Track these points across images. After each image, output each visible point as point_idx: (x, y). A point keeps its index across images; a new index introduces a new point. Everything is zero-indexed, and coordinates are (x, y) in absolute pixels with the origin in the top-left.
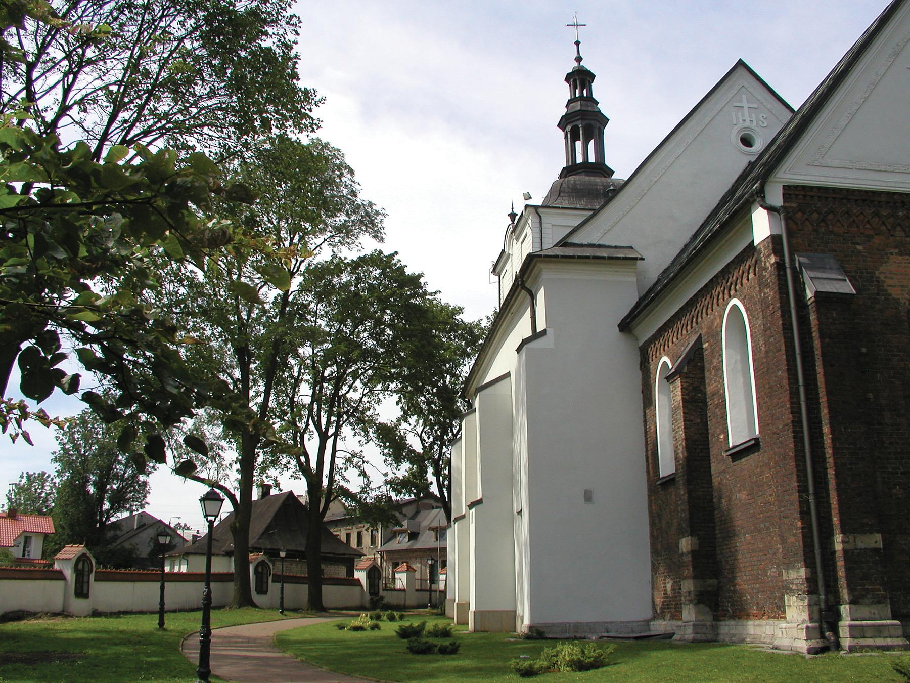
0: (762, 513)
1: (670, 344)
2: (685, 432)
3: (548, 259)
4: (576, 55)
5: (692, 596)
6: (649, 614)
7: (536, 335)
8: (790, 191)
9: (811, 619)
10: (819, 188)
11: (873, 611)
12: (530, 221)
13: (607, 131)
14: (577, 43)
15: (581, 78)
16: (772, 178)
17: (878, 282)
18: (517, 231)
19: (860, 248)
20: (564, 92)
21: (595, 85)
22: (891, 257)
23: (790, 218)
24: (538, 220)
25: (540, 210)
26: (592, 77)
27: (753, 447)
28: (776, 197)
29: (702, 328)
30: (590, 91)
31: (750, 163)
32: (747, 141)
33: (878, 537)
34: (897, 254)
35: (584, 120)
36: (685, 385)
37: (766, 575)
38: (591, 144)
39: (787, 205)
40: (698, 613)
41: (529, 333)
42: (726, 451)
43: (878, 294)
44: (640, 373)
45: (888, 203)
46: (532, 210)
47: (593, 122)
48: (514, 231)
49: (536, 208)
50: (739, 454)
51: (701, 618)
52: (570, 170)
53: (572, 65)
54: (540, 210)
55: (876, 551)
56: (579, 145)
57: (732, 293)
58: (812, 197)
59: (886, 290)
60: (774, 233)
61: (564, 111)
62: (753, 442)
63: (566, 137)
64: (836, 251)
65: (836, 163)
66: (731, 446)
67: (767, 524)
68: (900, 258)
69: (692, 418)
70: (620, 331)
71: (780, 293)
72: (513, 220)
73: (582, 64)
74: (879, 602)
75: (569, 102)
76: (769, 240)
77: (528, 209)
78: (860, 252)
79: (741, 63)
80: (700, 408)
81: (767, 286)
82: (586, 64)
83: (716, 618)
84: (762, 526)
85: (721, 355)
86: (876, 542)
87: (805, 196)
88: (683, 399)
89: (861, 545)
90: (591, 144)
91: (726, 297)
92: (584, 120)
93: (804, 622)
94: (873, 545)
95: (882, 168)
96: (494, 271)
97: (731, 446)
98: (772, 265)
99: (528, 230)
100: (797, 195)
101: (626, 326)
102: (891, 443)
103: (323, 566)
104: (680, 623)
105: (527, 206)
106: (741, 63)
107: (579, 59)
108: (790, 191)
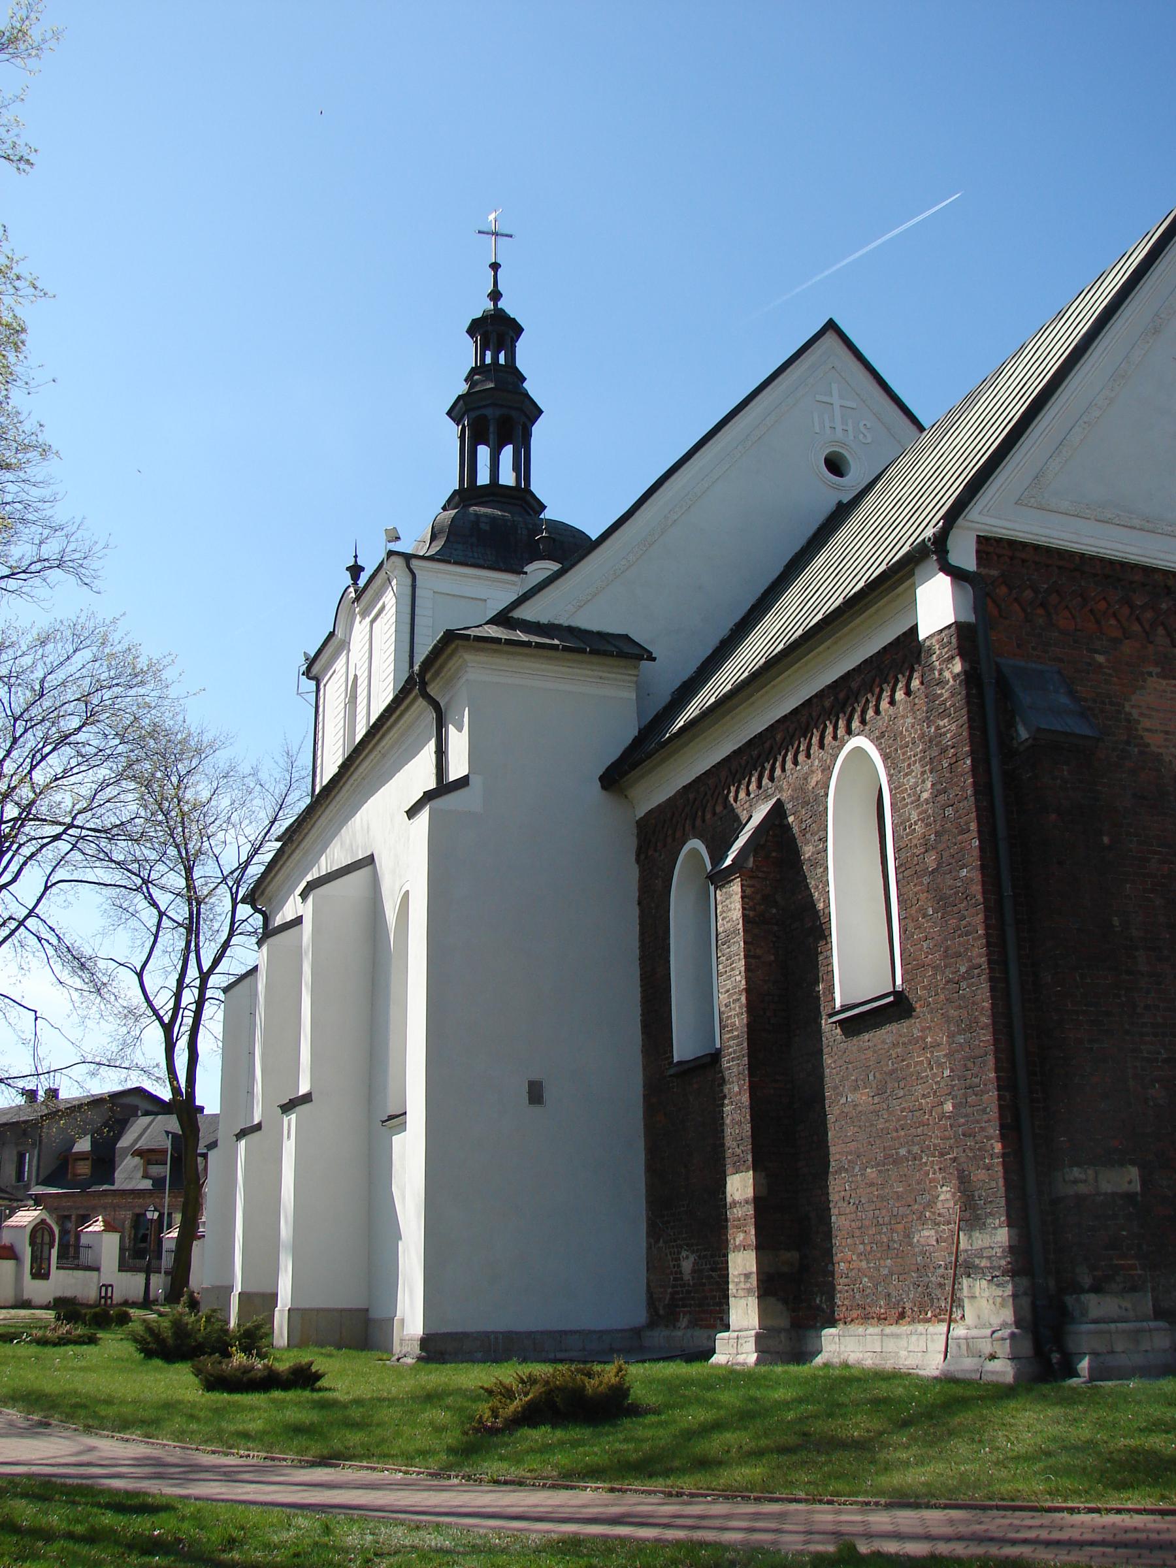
0: (912, 1126)
1: (708, 816)
2: (747, 979)
3: (482, 645)
6: (640, 1317)
7: (444, 788)
8: (987, 546)
9: (1018, 1323)
10: (1037, 548)
11: (1124, 1304)
12: (394, 582)
13: (539, 430)
14: (495, 266)
15: (496, 330)
16: (960, 521)
17: (1128, 721)
19: (1100, 659)
20: (465, 354)
22: (1149, 679)
23: (988, 595)
24: (409, 581)
25: (415, 563)
26: (518, 330)
27: (896, 1008)
28: (964, 555)
29: (781, 790)
30: (511, 356)
31: (840, 504)
33: (1134, 1172)
34: (1158, 676)
35: (496, 408)
36: (748, 891)
37: (911, 1244)
38: (507, 453)
39: (984, 571)
41: (432, 784)
42: (830, 1016)
43: (1128, 743)
44: (633, 873)
45: (1144, 585)
46: (399, 562)
47: (514, 414)
48: (358, 599)
49: (408, 557)
50: (859, 1023)
52: (466, 495)
54: (415, 563)
55: (1130, 1197)
56: (483, 452)
57: (855, 724)
58: (1023, 561)
59: (1142, 738)
60: (962, 620)
61: (463, 388)
62: (891, 999)
63: (462, 438)
64: (1061, 660)
66: (838, 1005)
67: (916, 1149)
68: (1164, 682)
69: (759, 952)
70: (604, 787)
71: (970, 727)
73: (500, 305)
74: (1134, 1289)
75: (474, 371)
76: (953, 629)
77: (393, 558)
78: (1100, 666)
79: (831, 326)
80: (789, 929)
81: (943, 714)
84: (903, 1152)
85: (824, 840)
86: (1130, 1182)
87: (1012, 558)
88: (744, 916)
89: (1106, 1187)
90: (507, 453)
91: (841, 732)
92: (496, 408)
93: (1004, 1325)
94: (1125, 1188)
95: (1136, 522)
96: (307, 673)
97: (838, 1005)
98: (955, 677)
99: (389, 599)
100: (999, 556)
101: (614, 778)
102: (1147, 1007)
105: (391, 553)
106: (831, 326)
107: (495, 295)
108: (987, 546)
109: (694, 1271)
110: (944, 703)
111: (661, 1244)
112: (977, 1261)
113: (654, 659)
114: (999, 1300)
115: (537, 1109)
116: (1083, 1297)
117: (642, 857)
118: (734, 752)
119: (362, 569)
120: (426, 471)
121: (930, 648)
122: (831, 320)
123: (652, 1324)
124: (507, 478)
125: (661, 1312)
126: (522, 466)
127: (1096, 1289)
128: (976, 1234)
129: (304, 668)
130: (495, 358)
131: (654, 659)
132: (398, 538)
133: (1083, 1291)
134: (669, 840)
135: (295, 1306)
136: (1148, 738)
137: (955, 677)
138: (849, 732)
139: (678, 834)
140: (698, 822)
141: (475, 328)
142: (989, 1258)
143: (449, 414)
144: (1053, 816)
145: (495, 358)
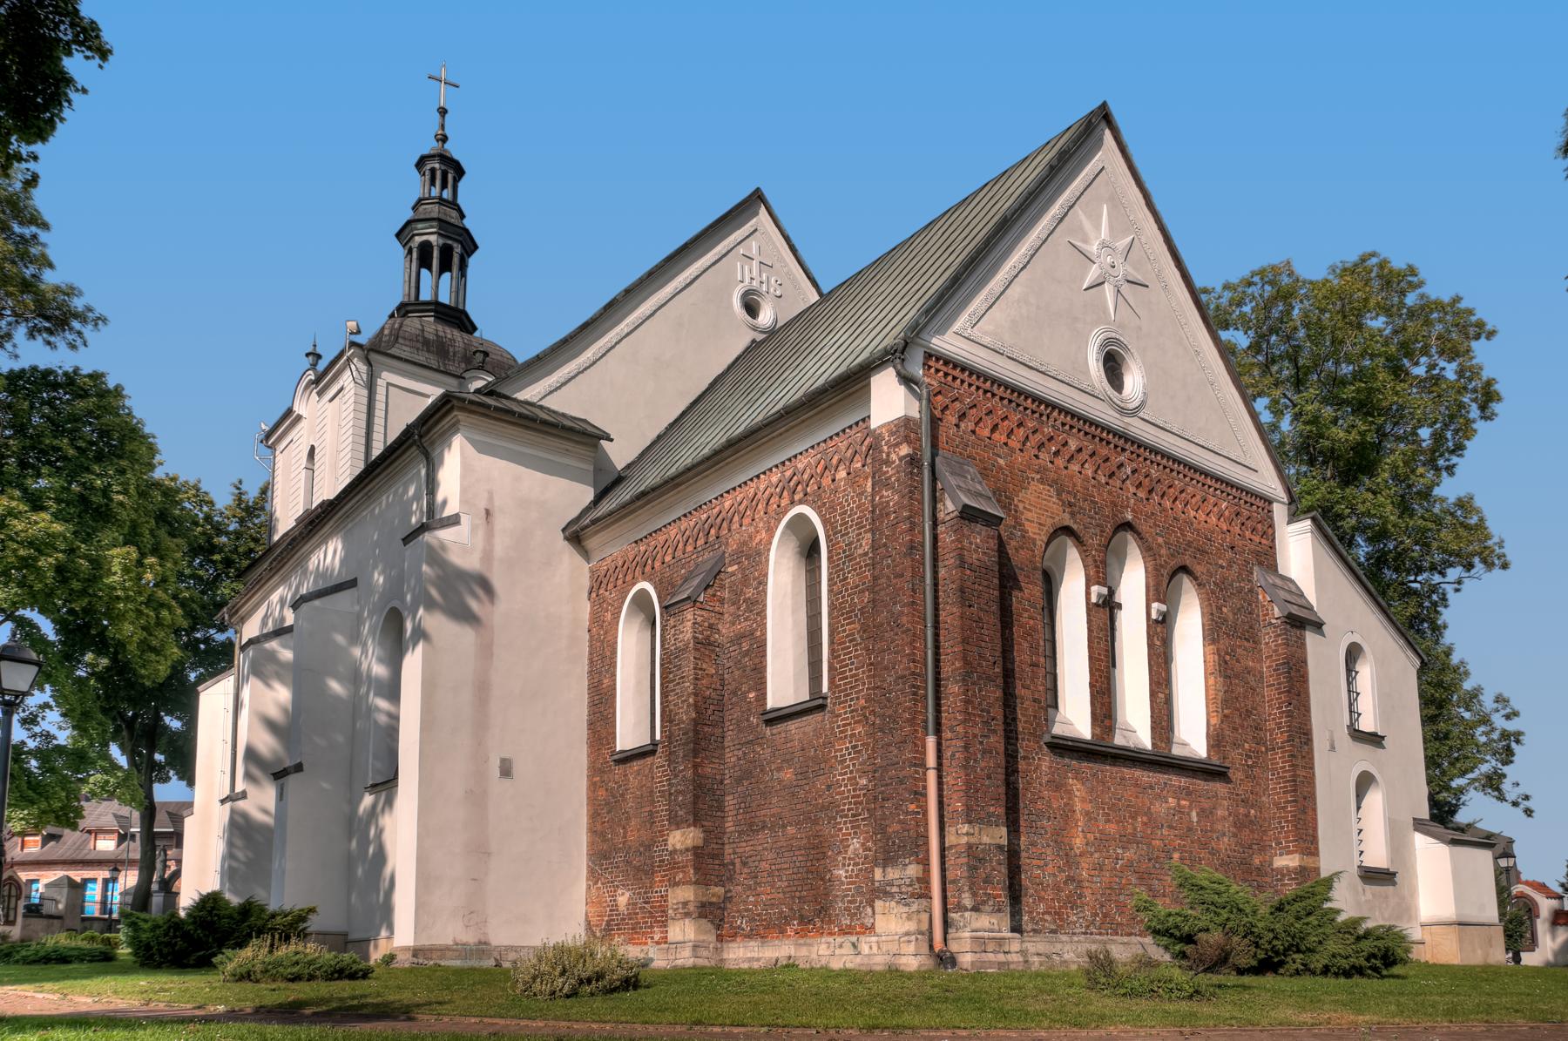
4: (436, 129)
5: (691, 908)
14: (443, 112)
15: (444, 168)
19: (1001, 462)
27: (815, 706)
32: (751, 309)
40: (698, 931)
51: (702, 938)
53: (429, 146)
55: (1000, 847)
65: (986, 340)
74: (999, 910)
81: (888, 486)
82: (454, 149)
83: (720, 938)
87: (946, 374)
97: (769, 706)
103: (1448, 490)
105: (353, 344)
115: (507, 782)
120: (380, 282)
122: (758, 190)
124: (445, 298)
126: (460, 288)
128: (889, 869)
134: (620, 582)
135: (425, 942)
136: (1028, 526)
138: (793, 503)
139: (629, 578)
140: (648, 568)
143: (398, 235)
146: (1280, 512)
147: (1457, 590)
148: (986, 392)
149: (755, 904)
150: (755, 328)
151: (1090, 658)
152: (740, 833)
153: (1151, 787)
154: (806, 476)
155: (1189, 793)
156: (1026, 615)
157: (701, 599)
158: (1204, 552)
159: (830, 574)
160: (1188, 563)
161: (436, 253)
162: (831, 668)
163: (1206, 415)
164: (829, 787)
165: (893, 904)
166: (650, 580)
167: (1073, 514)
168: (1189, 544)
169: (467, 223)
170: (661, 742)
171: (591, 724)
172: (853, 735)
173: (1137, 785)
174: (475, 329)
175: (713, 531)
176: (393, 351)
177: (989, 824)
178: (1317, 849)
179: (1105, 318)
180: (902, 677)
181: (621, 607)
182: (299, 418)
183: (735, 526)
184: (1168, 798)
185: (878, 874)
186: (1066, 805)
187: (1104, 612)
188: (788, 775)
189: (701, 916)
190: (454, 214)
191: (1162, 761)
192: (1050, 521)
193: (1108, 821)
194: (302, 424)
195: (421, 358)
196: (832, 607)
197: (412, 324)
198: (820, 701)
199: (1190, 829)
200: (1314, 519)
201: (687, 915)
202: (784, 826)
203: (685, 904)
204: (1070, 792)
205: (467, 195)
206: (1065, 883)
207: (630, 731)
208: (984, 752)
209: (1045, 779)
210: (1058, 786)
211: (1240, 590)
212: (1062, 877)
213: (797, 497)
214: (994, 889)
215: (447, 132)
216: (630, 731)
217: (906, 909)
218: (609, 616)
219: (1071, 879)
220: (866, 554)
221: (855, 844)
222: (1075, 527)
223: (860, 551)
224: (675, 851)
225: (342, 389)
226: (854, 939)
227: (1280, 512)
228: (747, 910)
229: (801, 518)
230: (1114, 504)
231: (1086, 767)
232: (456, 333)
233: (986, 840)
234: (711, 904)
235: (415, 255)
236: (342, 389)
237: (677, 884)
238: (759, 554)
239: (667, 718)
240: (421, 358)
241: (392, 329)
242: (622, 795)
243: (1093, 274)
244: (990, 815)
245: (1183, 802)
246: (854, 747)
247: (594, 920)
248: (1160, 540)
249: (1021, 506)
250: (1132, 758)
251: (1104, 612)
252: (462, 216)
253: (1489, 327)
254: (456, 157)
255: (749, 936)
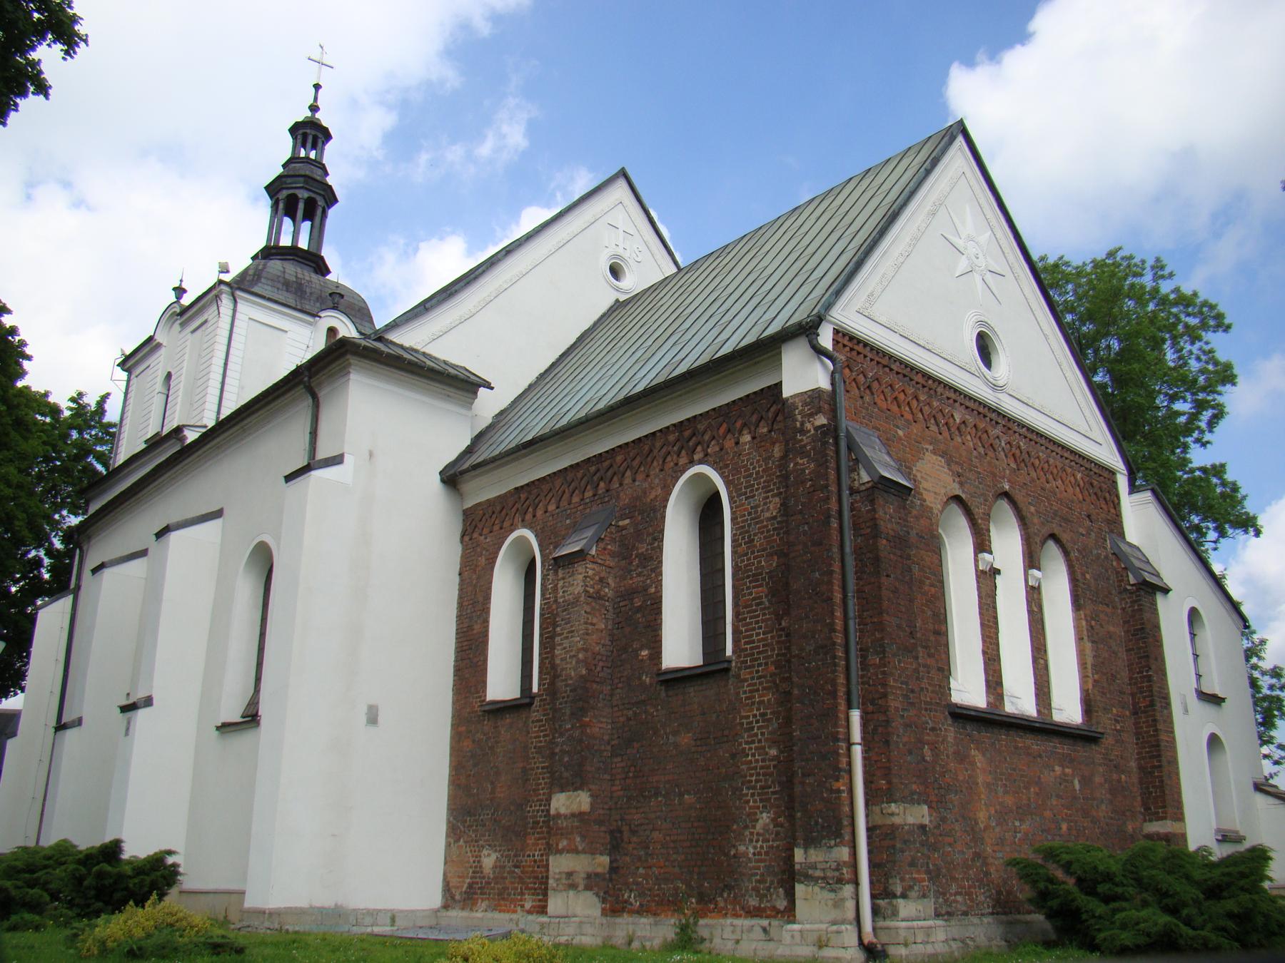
14: (317, 87)
15: (310, 133)
18: (185, 317)
19: (900, 433)
20: (284, 148)
21: (329, 147)
32: (615, 271)
35: (301, 191)
44: (454, 552)
53: (303, 114)
69: (595, 621)
72: (179, 297)
73: (318, 115)
74: (924, 896)
79: (623, 174)
81: (803, 453)
82: (323, 117)
87: (852, 349)
94: (918, 821)
103: (1199, 457)
104: (544, 919)
105: (221, 282)
107: (314, 108)
109: (495, 867)
110: (805, 446)
111: (461, 843)
112: (810, 872)
113: (1227, 328)
114: (830, 903)
115: (372, 729)
116: (894, 901)
117: (467, 538)
118: (571, 466)
119: (185, 291)
121: (793, 404)
123: (446, 907)
124: (303, 244)
125: (458, 897)
126: (317, 236)
127: (904, 896)
128: (812, 851)
129: (119, 361)
130: (307, 154)
131: (1227, 328)
132: (228, 272)
133: (895, 896)
137: (816, 429)
139: (506, 524)
141: (295, 130)
142: (823, 870)
144: (884, 542)
145: (307, 154)
146: (1122, 482)
147: (1215, 549)
148: (885, 366)
149: (646, 877)
150: (618, 290)
151: (982, 625)
152: (629, 798)
153: (1040, 756)
154: (707, 437)
155: (1072, 761)
156: (928, 582)
157: (593, 552)
158: (1067, 520)
159: (734, 535)
160: (1056, 532)
161: (301, 206)
162: (736, 631)
163: (1048, 391)
164: (733, 756)
165: (817, 889)
166: (531, 528)
167: (961, 484)
168: (1055, 513)
169: (330, 180)
170: (538, 695)
171: (458, 670)
172: (761, 702)
173: (1028, 754)
174: (328, 272)
175: (602, 484)
176: (255, 289)
177: (912, 802)
178: (1182, 814)
179: (946, 300)
180: (822, 647)
181: (497, 553)
182: (159, 346)
183: (628, 480)
184: (1054, 769)
185: (799, 855)
186: (970, 776)
187: (987, 578)
188: (685, 739)
189: (588, 888)
190: (320, 172)
191: (1042, 728)
192: (943, 491)
193: (1006, 792)
194: (162, 351)
195: (281, 297)
196: (736, 569)
197: (275, 265)
198: (725, 665)
199: (1075, 798)
200: (1153, 491)
201: (573, 886)
202: (681, 795)
203: (569, 874)
204: (973, 763)
205: (331, 155)
206: (973, 860)
207: (502, 683)
208: (907, 726)
209: (951, 750)
210: (962, 758)
211: (1098, 556)
212: (969, 854)
213: (696, 457)
214: (918, 872)
215: (319, 103)
216: (502, 683)
217: (832, 895)
218: (482, 561)
219: (977, 855)
220: (774, 518)
221: (765, 818)
222: (963, 496)
223: (767, 515)
224: (558, 815)
225: (206, 321)
226: (765, 922)
227: (1122, 482)
228: (638, 884)
229: (700, 477)
230: (994, 475)
231: (986, 736)
232: (314, 276)
233: (911, 820)
234: (597, 875)
235: (281, 205)
236: (206, 321)
237: (560, 852)
238: (654, 510)
239: (549, 667)
240: (281, 297)
241: (256, 269)
242: (491, 748)
243: (963, 265)
244: (913, 793)
245: (1067, 770)
246: (762, 715)
247: (454, 881)
248: (1032, 509)
249: (919, 475)
250: (1019, 725)
251: (987, 578)
252: (327, 174)
253: (1226, 321)
254: (324, 124)
255: (640, 912)
